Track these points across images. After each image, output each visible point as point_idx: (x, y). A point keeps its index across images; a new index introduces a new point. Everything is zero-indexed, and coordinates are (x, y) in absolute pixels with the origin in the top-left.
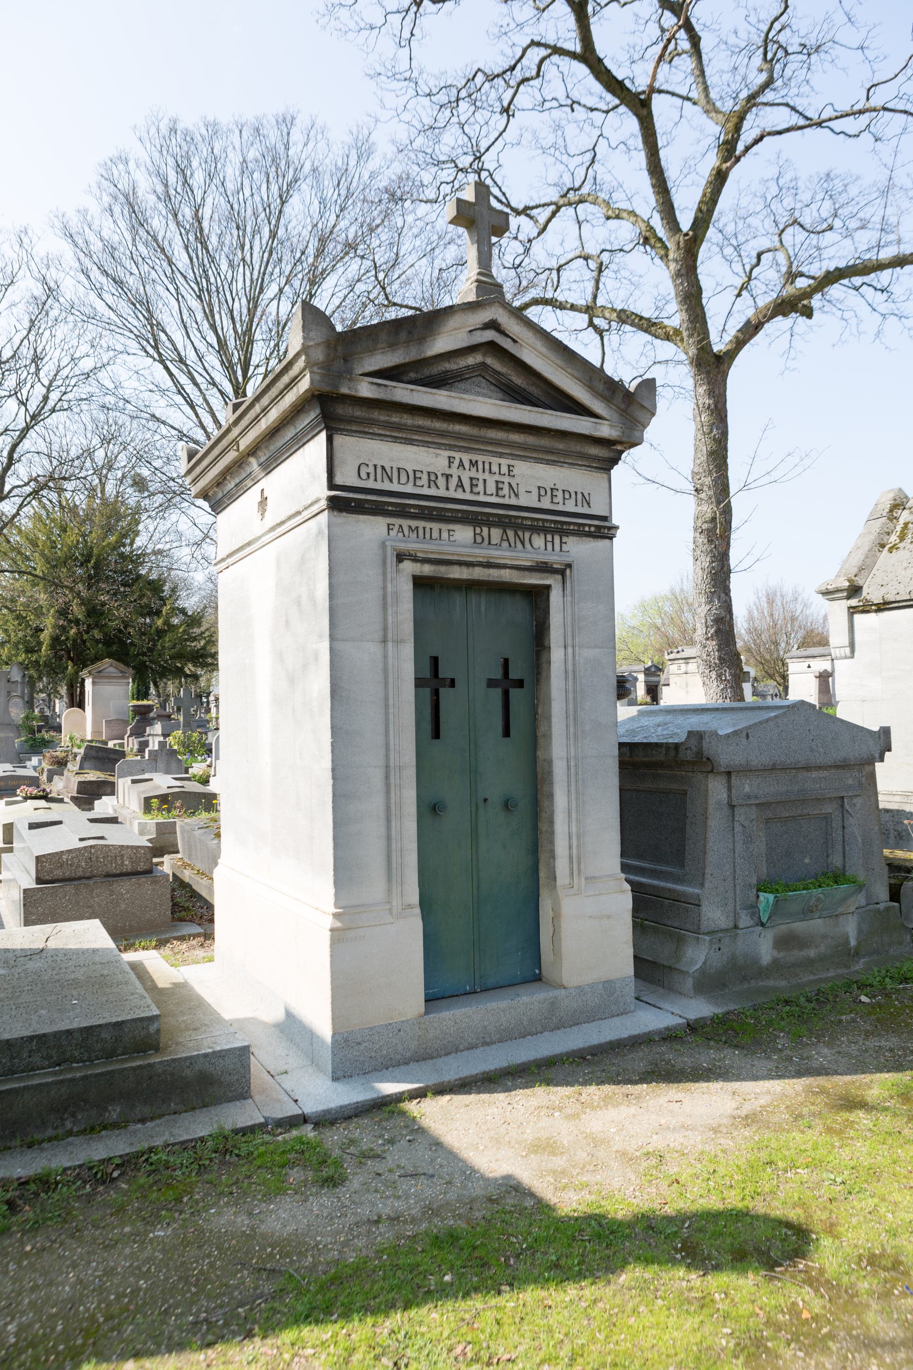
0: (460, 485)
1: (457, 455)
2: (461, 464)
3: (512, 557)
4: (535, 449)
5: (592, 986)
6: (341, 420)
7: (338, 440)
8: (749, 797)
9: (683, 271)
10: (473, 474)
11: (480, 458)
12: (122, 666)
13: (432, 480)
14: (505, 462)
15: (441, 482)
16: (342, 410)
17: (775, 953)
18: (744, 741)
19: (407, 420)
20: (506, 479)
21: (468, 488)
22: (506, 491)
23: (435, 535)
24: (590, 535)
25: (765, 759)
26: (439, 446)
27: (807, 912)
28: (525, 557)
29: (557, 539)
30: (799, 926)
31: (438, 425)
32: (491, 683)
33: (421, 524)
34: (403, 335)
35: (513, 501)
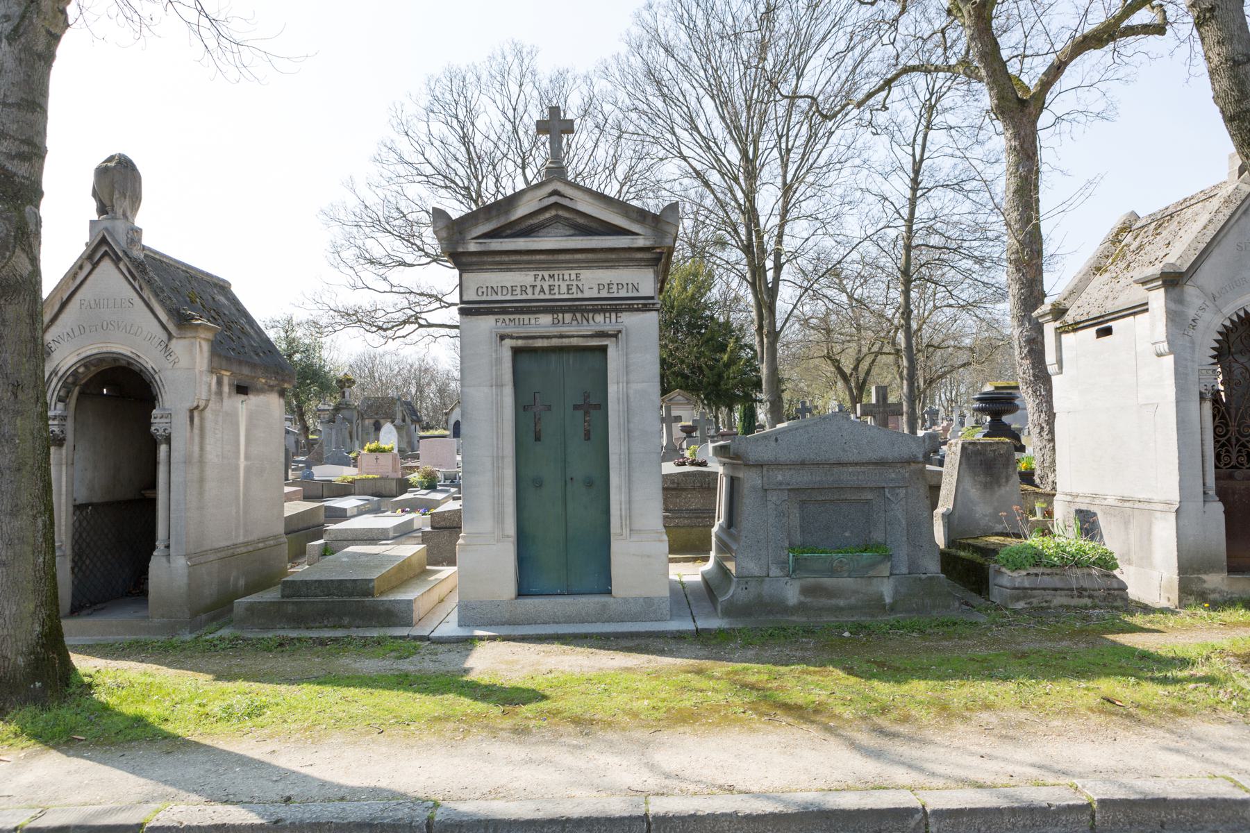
0: (542, 290)
1: (540, 273)
2: (543, 278)
3: (576, 330)
4: (595, 261)
5: (635, 599)
6: (466, 265)
7: (465, 275)
8: (781, 484)
9: (976, 35)
10: (551, 283)
11: (556, 273)
12: (688, 395)
13: (524, 289)
14: (573, 272)
15: (529, 290)
16: (464, 260)
17: (802, 598)
18: (773, 444)
19: (506, 258)
20: (574, 283)
21: (547, 291)
22: (574, 289)
23: (526, 322)
24: (638, 310)
25: (794, 457)
26: (529, 270)
27: (832, 572)
28: (587, 329)
29: (613, 315)
30: (828, 581)
31: (525, 258)
32: (576, 407)
33: (516, 317)
34: (494, 213)
35: (580, 295)
